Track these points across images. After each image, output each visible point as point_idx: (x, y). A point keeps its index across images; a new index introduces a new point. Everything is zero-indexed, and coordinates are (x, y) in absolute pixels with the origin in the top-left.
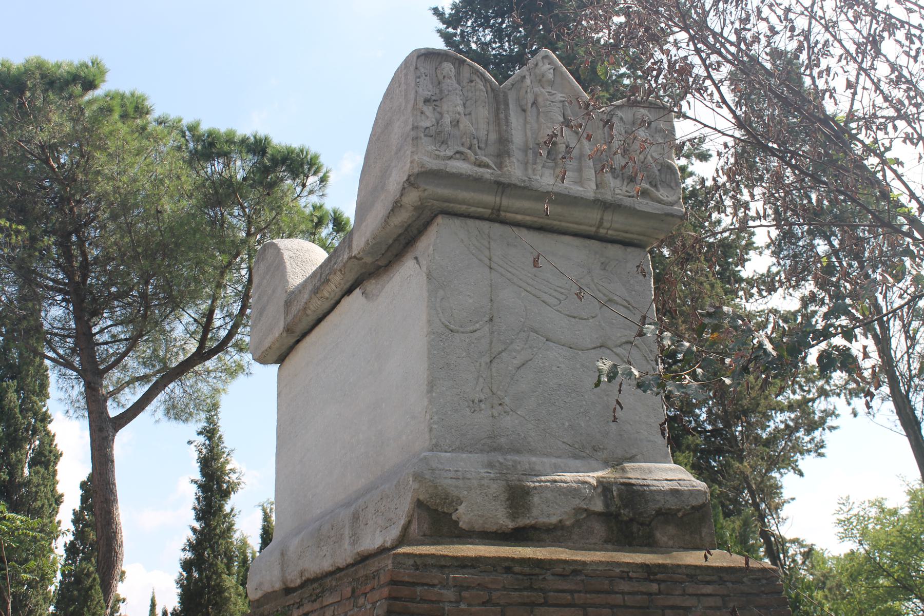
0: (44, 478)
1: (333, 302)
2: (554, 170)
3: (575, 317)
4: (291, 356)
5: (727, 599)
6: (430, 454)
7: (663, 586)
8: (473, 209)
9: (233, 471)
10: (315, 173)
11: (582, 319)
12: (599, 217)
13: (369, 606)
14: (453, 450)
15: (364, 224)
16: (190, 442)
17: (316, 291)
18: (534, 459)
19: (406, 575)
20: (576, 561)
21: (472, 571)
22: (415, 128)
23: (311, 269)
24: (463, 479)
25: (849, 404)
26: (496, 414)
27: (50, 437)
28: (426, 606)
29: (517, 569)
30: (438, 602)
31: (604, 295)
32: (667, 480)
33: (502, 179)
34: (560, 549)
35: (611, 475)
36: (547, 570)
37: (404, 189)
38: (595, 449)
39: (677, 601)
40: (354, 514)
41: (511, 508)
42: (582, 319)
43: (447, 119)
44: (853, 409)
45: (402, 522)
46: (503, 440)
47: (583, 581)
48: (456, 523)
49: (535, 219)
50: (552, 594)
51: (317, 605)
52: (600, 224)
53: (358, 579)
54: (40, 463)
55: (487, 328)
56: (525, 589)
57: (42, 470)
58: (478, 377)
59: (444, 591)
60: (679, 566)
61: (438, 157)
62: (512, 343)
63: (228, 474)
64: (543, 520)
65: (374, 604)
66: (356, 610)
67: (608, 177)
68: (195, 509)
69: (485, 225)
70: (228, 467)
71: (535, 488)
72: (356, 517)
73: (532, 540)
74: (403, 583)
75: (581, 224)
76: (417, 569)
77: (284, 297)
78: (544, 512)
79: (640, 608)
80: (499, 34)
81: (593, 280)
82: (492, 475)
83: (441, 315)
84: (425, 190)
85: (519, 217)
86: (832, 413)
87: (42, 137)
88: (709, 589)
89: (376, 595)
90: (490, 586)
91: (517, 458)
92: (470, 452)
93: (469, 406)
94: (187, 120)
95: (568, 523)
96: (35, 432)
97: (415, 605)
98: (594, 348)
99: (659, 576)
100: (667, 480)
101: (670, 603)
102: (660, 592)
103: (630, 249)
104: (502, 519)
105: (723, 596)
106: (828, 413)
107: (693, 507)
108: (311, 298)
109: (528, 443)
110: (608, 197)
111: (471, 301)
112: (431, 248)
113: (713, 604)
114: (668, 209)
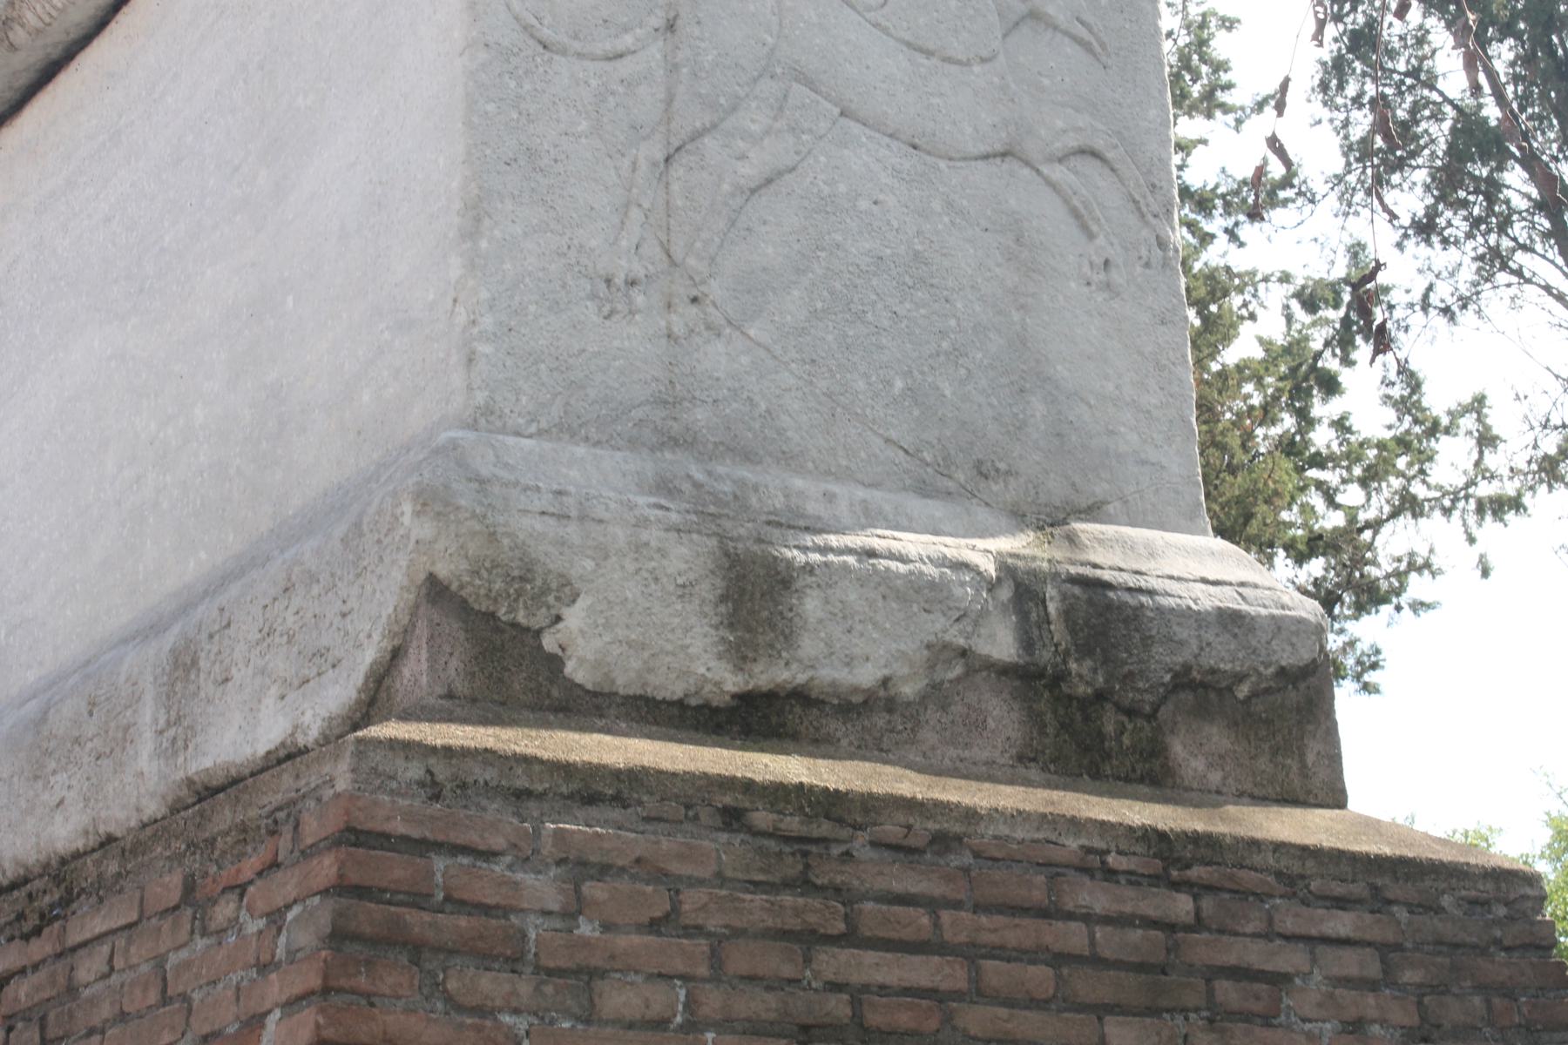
3: (929, 53)
5: (1394, 957)
7: (1207, 904)
11: (948, 60)
13: (253, 926)
14: (540, 433)
18: (798, 483)
19: (396, 814)
20: (937, 804)
21: (616, 814)
25: (1472, 540)
26: (679, 329)
28: (463, 922)
29: (762, 818)
30: (504, 911)
32: (1204, 581)
34: (889, 769)
35: (1038, 552)
36: (857, 827)
39: (1254, 954)
40: (175, 654)
41: (731, 626)
42: (948, 60)
44: (1482, 556)
45: (369, 655)
46: (701, 415)
47: (966, 870)
48: (555, 663)
50: (869, 906)
51: (41, 948)
53: (211, 842)
55: (655, 51)
56: (787, 885)
58: (627, 205)
59: (526, 878)
60: (1254, 844)
62: (734, 109)
64: (831, 674)
65: (275, 917)
66: (200, 943)
71: (809, 569)
72: (184, 664)
73: (795, 737)
74: (383, 840)
76: (436, 797)
78: (839, 650)
79: (1140, 968)
82: (674, 517)
88: (1341, 924)
89: (286, 885)
90: (675, 867)
91: (745, 473)
92: (598, 443)
93: (593, 296)
95: (908, 690)
97: (427, 917)
98: (986, 157)
99: (1196, 872)
100: (1204, 581)
101: (1231, 959)
102: (1199, 924)
104: (701, 663)
105: (1384, 949)
107: (1282, 672)
109: (781, 432)
113: (1353, 971)
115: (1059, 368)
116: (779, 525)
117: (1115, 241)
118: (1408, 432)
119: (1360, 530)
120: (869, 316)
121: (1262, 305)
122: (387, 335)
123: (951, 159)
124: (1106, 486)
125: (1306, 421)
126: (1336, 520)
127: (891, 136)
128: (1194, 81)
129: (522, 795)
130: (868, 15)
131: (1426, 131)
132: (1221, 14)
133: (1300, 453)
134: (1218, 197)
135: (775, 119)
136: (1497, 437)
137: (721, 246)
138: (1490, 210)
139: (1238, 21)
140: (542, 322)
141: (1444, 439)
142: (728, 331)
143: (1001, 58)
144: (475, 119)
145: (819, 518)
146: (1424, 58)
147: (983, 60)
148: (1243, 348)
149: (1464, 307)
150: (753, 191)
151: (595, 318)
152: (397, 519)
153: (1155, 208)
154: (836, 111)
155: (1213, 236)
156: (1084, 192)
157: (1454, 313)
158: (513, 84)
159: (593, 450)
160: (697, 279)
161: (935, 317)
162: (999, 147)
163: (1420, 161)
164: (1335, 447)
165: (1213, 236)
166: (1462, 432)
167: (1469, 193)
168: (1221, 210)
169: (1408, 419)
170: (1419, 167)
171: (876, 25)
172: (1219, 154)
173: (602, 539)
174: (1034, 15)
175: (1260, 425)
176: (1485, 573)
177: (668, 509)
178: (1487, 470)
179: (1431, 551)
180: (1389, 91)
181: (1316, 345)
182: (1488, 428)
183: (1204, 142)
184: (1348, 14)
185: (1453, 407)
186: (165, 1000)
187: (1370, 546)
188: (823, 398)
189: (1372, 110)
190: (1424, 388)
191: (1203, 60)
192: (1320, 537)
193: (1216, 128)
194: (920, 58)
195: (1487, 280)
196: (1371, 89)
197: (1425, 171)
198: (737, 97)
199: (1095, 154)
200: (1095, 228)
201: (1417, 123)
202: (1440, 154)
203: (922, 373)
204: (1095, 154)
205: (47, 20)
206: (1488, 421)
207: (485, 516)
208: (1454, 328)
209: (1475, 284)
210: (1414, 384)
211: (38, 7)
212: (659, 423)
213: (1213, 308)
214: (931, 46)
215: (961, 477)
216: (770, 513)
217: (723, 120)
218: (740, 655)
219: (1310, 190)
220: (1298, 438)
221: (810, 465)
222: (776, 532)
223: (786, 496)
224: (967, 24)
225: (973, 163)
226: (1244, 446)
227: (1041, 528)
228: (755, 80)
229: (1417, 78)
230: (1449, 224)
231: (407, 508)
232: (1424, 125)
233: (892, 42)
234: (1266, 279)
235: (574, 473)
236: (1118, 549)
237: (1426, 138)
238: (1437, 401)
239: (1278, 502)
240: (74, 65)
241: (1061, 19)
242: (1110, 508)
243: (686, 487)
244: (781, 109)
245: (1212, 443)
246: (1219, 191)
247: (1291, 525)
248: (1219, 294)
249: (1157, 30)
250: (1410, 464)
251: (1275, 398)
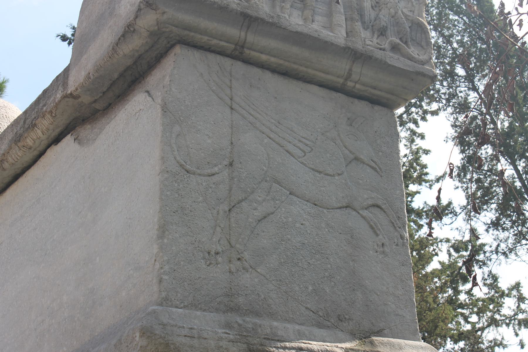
1: (36, 153)
2: (303, 12)
3: (320, 172)
6: (160, 308)
8: (214, 42)
11: (327, 175)
12: (348, 67)
14: (185, 307)
15: (85, 57)
17: (18, 139)
18: (275, 324)
24: (199, 338)
25: (517, 335)
26: (233, 269)
31: (351, 152)
33: (249, 12)
35: (360, 348)
37: (139, 10)
42: (327, 175)
44: (521, 340)
46: (241, 300)
49: (281, 62)
55: (226, 173)
58: (216, 226)
62: (253, 192)
67: (358, 25)
69: (227, 62)
75: (328, 73)
81: (339, 135)
82: (231, 337)
83: (176, 153)
84: (164, 13)
85: (264, 57)
91: (257, 321)
92: (204, 310)
93: (204, 258)
103: (377, 108)
108: (10, 148)
110: (359, 46)
111: (209, 141)
112: (167, 79)
114: (419, 67)
115: (367, 282)
116: (268, 339)
117: (386, 237)
118: (493, 296)
119: (477, 331)
120: (300, 264)
121: (440, 250)
122: (131, 272)
123: (328, 209)
124: (384, 323)
125: (457, 292)
126: (468, 327)
127: (307, 201)
128: (415, 172)
130: (299, 160)
131: (495, 191)
132: (424, 148)
133: (455, 303)
134: (424, 212)
135: (267, 196)
136: (525, 298)
137: (248, 240)
138: (518, 218)
139: (430, 151)
140: (186, 267)
141: (506, 298)
142: (250, 270)
143: (345, 173)
144: (163, 197)
145: (283, 336)
146: (494, 165)
147: (339, 175)
148: (434, 265)
149: (511, 252)
150: (259, 221)
151: (204, 266)
152: (134, 338)
153: (400, 225)
154: (288, 193)
155: (422, 226)
156: (375, 220)
157: (507, 254)
158: (176, 185)
159: (203, 313)
160: (240, 252)
161: (323, 264)
162: (345, 204)
163: (493, 201)
164: (467, 301)
165: (422, 226)
166: (512, 296)
167: (511, 212)
168: (425, 217)
169: (493, 291)
170: (493, 203)
171: (302, 163)
172: (424, 198)
173: (206, 345)
174: (357, 159)
175: (440, 294)
176: (522, 347)
177: (229, 334)
178: (521, 309)
179: (503, 339)
180: (481, 177)
181: (460, 264)
182: (521, 294)
183: (419, 193)
184: (466, 150)
185: (510, 287)
187: (480, 337)
188: (284, 294)
189: (476, 183)
190: (499, 280)
191: (418, 164)
192: (462, 334)
193: (424, 188)
194: (317, 174)
195: (519, 243)
196: (475, 176)
197: (495, 205)
198: (254, 188)
199: (378, 206)
200: (378, 232)
201: (492, 188)
202: (501, 198)
203: (319, 284)
204: (378, 206)
205: (16, 160)
206: (521, 292)
207: (165, 337)
208: (507, 260)
209: (514, 244)
210: (495, 278)
211: (13, 156)
212: (226, 303)
213: (422, 252)
214: (321, 170)
215: (332, 321)
216: (265, 335)
217: (248, 196)
219: (455, 211)
220: (454, 298)
221: (279, 317)
222: (268, 342)
223: (271, 329)
224: (333, 162)
225: (336, 210)
226: (434, 302)
227: (361, 339)
228: (260, 183)
229: (491, 172)
230: (504, 223)
231: (138, 335)
232: (494, 188)
233: (307, 169)
234: (441, 241)
235: (196, 321)
236: (388, 347)
237: (495, 193)
238: (504, 284)
239: (447, 321)
240: (25, 175)
241: (366, 160)
242: (385, 332)
243: (236, 326)
244: (269, 192)
245: (423, 300)
246: (424, 210)
247: (452, 329)
248: (424, 247)
249: (399, 163)
250: (494, 308)
251: (445, 283)
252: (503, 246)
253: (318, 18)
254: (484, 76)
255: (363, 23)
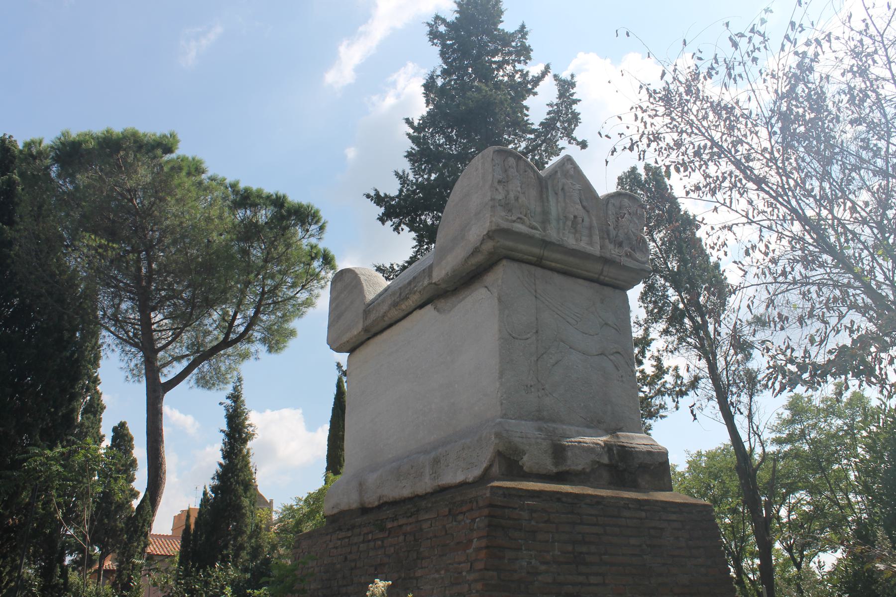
0: (92, 423)
4: (361, 348)
8: (526, 257)
9: (250, 425)
10: (316, 223)
14: (515, 419)
16: (221, 404)
17: (395, 305)
18: (564, 427)
22: (493, 199)
23: (380, 289)
27: (98, 395)
29: (564, 499)
33: (547, 239)
37: (483, 239)
38: (599, 422)
43: (512, 195)
45: (485, 465)
48: (522, 467)
51: (411, 520)
52: (601, 274)
54: (90, 412)
57: (92, 417)
61: (507, 220)
63: (246, 428)
64: (573, 467)
65: (473, 520)
68: (222, 450)
69: (533, 269)
70: (247, 422)
71: (569, 446)
72: (436, 461)
77: (363, 307)
78: (578, 463)
80: (449, 139)
85: (553, 264)
86: (662, 407)
87: (130, 184)
88: (674, 517)
91: (554, 425)
94: (230, 180)
95: (588, 470)
96: (88, 390)
99: (645, 508)
103: (617, 291)
104: (549, 466)
106: (662, 407)
108: (390, 309)
110: (608, 255)
112: (500, 281)
129: (520, 496)
174: (606, 324)
186: (446, 534)
218: (556, 464)
231: (493, 437)
252: (670, 346)
253: (583, 238)
254: (660, 232)
255: (609, 239)
